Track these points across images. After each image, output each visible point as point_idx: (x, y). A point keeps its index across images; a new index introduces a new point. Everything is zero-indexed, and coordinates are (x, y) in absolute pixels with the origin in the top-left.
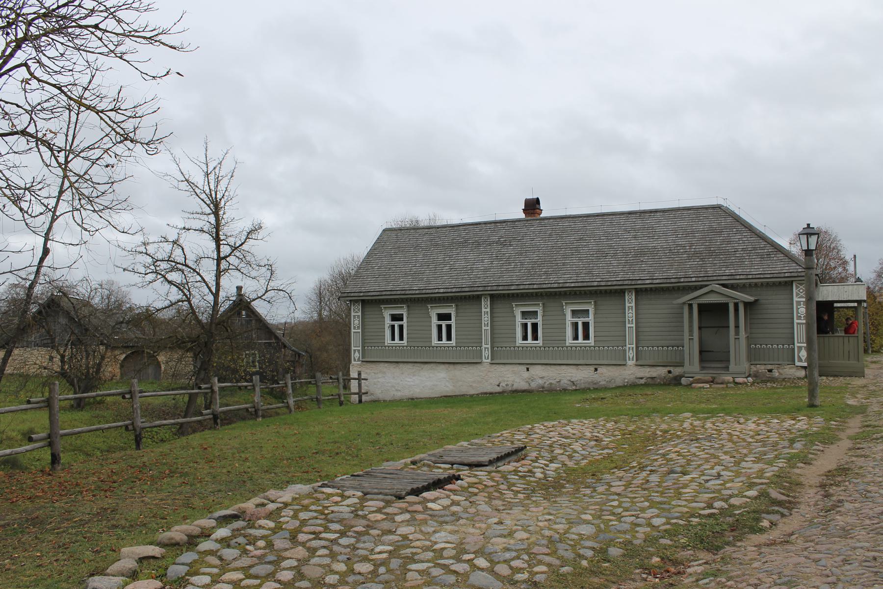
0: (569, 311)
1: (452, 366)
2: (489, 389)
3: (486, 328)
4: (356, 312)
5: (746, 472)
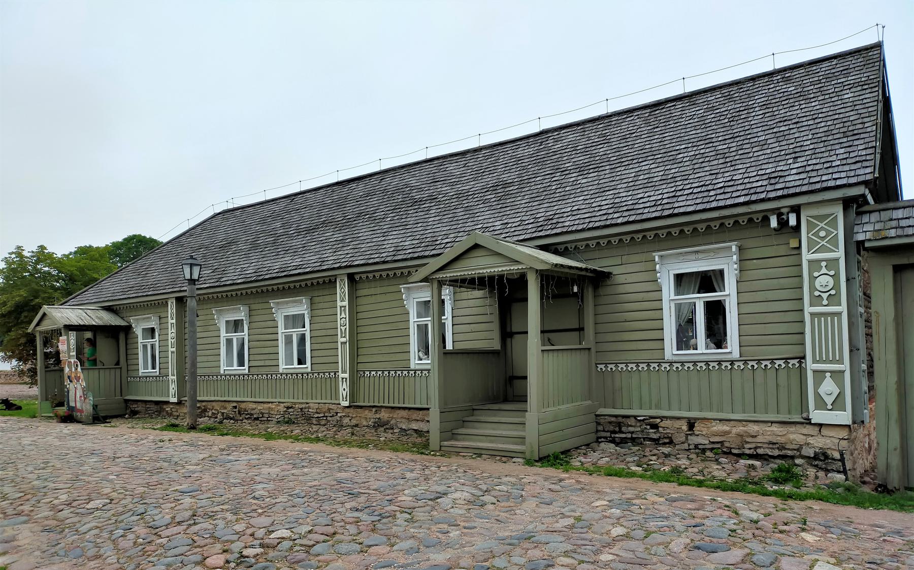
0: (283, 317)
4: (822, 249)
5: (225, 458)
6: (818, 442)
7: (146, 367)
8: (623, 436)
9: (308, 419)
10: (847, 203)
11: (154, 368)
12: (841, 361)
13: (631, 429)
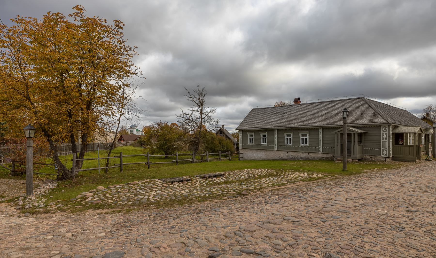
1: (266, 151)
2: (276, 158)
3: (276, 139)
12: (387, 148)
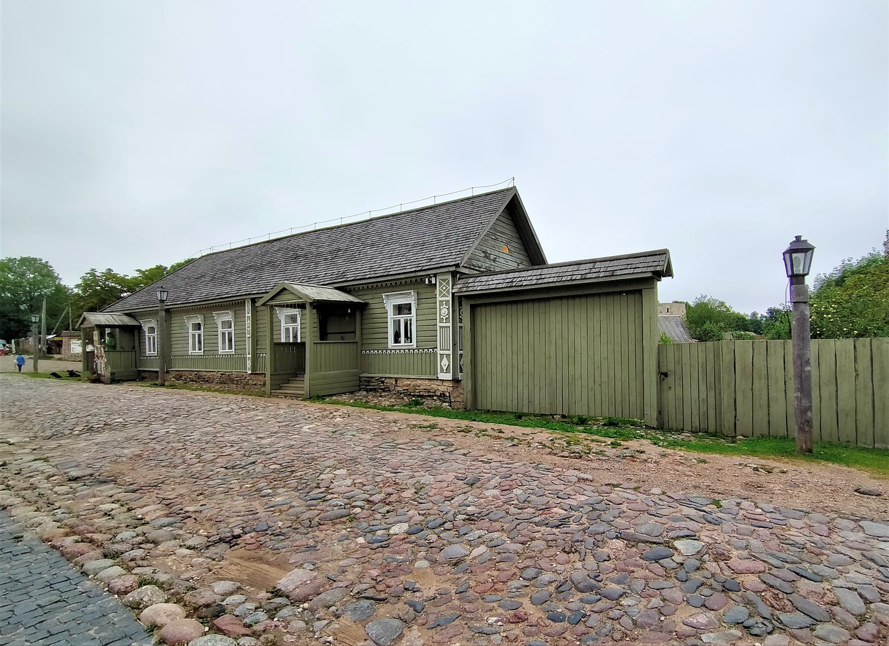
6: (442, 389)
7: (194, 349)
8: (370, 387)
9: (232, 381)
10: (454, 274)
11: (154, 351)
13: (374, 384)
